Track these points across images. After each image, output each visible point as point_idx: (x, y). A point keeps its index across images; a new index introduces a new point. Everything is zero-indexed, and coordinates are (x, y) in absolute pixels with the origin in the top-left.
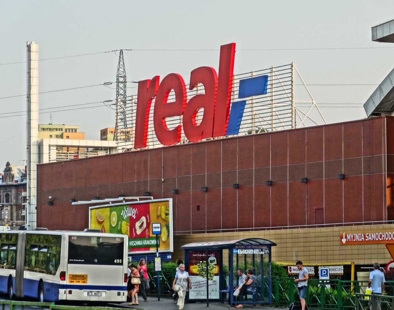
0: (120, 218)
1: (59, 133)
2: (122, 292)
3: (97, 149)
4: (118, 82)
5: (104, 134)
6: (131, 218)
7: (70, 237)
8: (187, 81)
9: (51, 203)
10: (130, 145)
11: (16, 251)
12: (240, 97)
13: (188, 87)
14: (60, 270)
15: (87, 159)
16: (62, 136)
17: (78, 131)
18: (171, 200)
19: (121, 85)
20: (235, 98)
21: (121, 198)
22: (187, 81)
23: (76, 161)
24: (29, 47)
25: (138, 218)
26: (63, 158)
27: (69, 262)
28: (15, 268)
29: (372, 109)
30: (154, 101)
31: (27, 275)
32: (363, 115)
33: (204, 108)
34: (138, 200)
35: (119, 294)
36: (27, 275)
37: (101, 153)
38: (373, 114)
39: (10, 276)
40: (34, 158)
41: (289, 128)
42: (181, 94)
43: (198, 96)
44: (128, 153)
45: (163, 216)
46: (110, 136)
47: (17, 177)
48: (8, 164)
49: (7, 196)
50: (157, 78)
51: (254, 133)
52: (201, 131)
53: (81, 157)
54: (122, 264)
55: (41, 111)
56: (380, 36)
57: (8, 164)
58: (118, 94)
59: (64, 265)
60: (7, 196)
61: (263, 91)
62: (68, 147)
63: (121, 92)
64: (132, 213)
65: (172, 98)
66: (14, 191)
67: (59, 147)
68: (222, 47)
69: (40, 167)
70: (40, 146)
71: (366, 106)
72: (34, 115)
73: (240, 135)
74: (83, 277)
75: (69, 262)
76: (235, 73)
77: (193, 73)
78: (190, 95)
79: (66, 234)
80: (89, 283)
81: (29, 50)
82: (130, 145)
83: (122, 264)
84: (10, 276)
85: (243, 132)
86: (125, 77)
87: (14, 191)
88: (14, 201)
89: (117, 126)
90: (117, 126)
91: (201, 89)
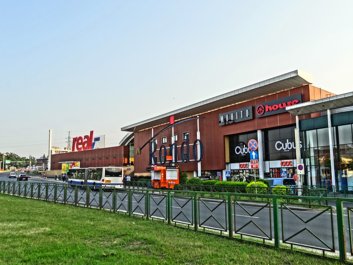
0: (69, 166)
1: (55, 148)
2: (121, 185)
3: (63, 152)
4: (69, 138)
5: (65, 148)
6: (71, 166)
7: (105, 168)
8: (83, 138)
9: (54, 163)
10: (71, 151)
11: (84, 174)
12: (94, 141)
13: (83, 139)
14: (102, 179)
15: (62, 154)
16: (56, 149)
17: (268, 106)
18: (79, 162)
19: (69, 139)
20: (93, 142)
21: (69, 162)
22: (83, 138)
23: (59, 154)
24: (50, 130)
25: (72, 166)
26: (56, 153)
27: (105, 176)
28: (84, 179)
29: (121, 144)
30: (76, 142)
31: (89, 181)
32: (118, 145)
33: (79, 146)
34: (72, 162)
35: (121, 186)
36: (89, 181)
37: (65, 152)
38: (121, 145)
39: (82, 182)
40: (50, 153)
41: (104, 148)
42: (82, 141)
43: (85, 141)
44: (70, 153)
45: (78, 165)
46: (66, 149)
47: (46, 157)
48: (44, 154)
49: (44, 161)
50: (77, 137)
51: (97, 149)
52: (86, 148)
53: (60, 153)
54: (121, 177)
55: (52, 144)
56: (123, 130)
57: (44, 154)
58: (68, 140)
59: (104, 177)
60: (44, 161)
61: (99, 140)
62: (57, 151)
63: (69, 140)
64: (71, 165)
65: (80, 141)
66: (45, 160)
67: (56, 151)
68: (91, 132)
69: (52, 156)
70: (52, 151)
71: (119, 143)
72: (50, 144)
73: (94, 149)
74: (109, 181)
75: (105, 176)
76: (93, 136)
77: (84, 136)
78: (84, 141)
79: (104, 169)
80: (111, 183)
81: (50, 131)
82: (71, 151)
83: (121, 177)
84: (82, 182)
85: (94, 148)
86: (70, 137)
87: (45, 160)
88: (45, 162)
89: (68, 147)
90: (68, 147)
91: (86, 140)
